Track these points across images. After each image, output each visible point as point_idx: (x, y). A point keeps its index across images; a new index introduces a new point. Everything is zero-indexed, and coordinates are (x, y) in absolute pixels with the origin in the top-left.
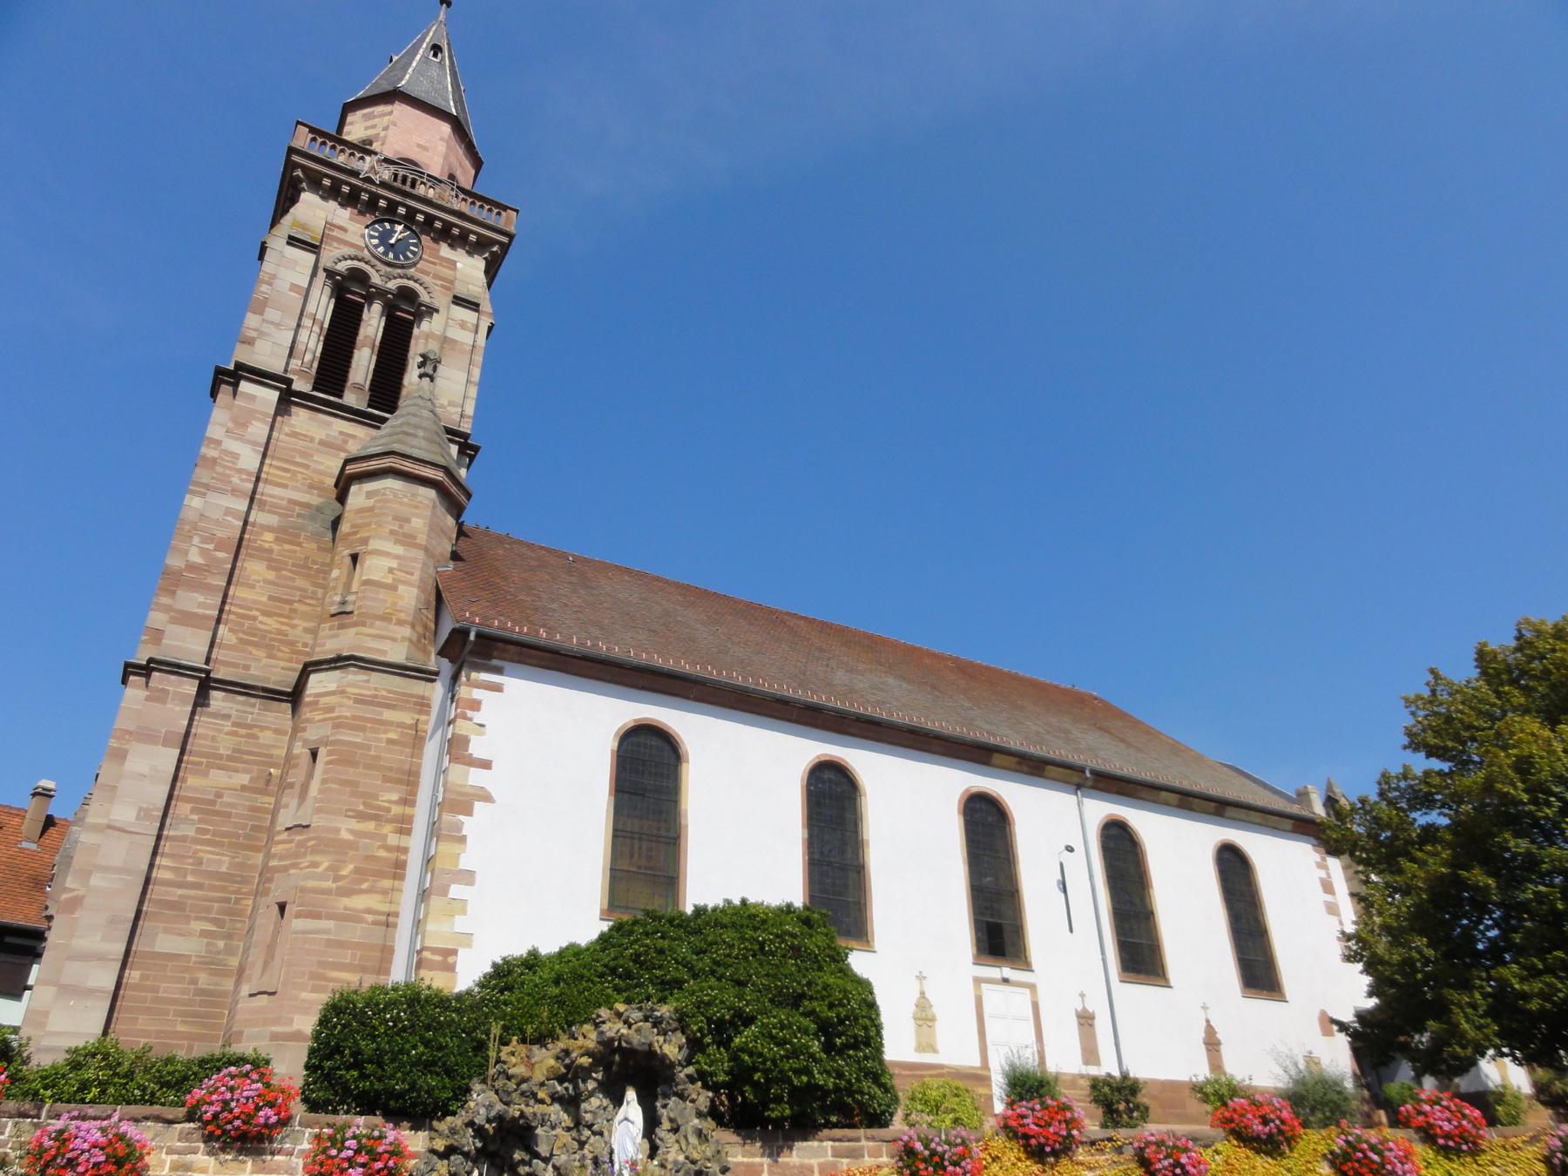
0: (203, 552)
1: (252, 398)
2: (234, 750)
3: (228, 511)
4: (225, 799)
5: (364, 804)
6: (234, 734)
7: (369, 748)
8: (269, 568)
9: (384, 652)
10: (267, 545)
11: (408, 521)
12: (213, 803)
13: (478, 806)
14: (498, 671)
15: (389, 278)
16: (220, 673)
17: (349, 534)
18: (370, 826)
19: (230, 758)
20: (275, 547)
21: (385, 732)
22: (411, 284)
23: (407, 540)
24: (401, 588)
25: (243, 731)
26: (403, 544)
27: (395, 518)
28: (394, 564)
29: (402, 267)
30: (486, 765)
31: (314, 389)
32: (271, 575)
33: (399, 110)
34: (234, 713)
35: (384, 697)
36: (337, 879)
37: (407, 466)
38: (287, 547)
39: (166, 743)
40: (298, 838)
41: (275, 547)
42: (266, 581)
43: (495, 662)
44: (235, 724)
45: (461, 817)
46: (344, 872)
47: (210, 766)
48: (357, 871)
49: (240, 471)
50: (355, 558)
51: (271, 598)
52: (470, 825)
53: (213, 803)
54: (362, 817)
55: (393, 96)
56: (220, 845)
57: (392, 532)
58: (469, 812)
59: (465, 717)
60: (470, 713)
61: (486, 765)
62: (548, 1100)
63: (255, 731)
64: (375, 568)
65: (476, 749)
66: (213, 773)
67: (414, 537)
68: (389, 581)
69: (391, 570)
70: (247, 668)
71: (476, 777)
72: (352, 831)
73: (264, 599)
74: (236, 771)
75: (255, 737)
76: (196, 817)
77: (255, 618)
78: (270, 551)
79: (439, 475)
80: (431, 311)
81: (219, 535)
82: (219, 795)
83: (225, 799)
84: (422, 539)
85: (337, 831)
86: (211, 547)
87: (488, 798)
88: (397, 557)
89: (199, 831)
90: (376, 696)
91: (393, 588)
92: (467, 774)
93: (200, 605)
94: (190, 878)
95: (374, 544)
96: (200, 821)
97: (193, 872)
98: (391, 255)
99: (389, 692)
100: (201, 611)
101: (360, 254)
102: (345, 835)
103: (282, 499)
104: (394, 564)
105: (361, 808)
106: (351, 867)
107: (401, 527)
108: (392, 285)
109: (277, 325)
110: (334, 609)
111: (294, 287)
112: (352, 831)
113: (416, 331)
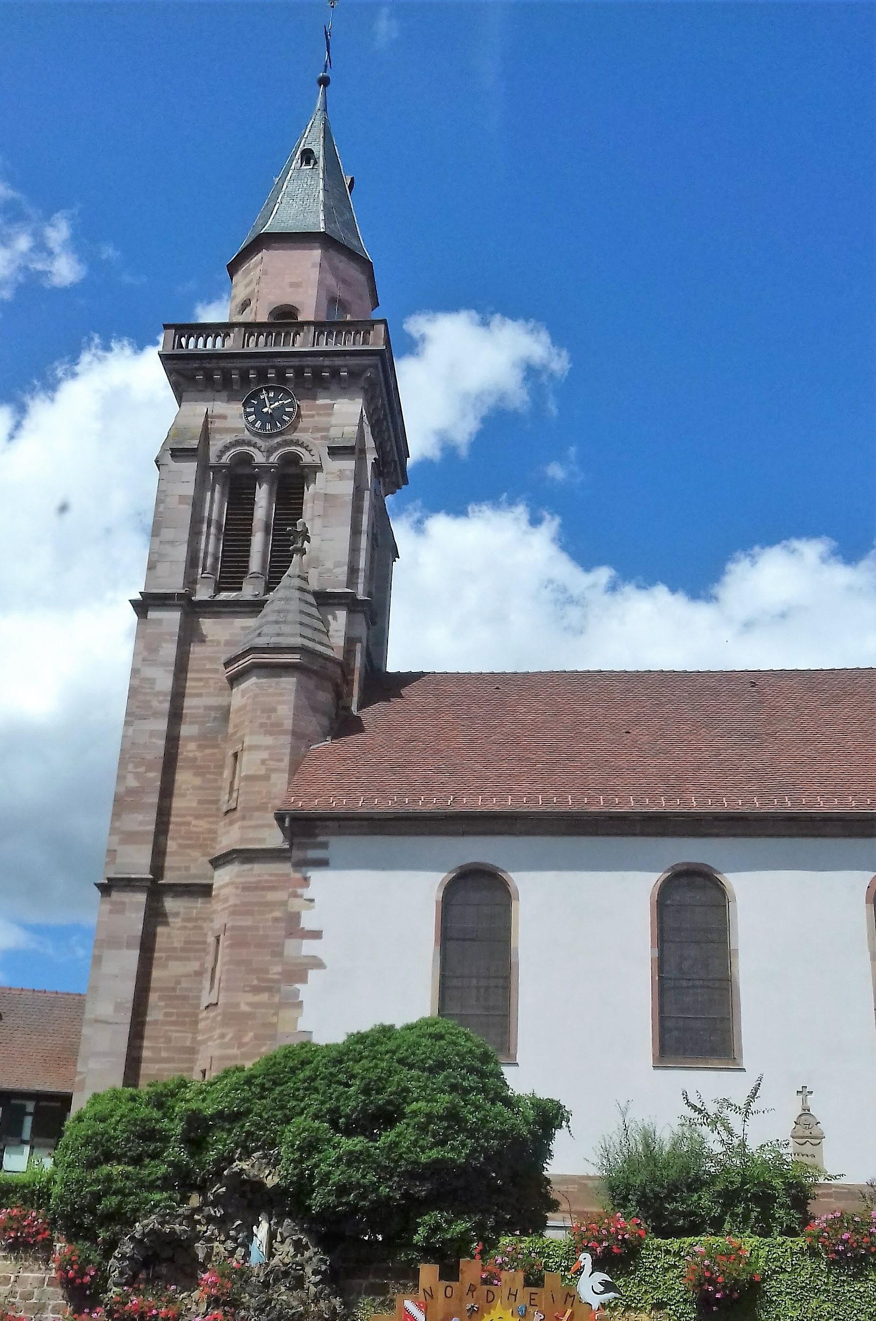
0: (137, 776)
1: (159, 622)
2: (187, 942)
3: (152, 734)
4: (184, 985)
5: (258, 979)
6: (185, 928)
7: (257, 928)
8: (196, 775)
9: (263, 840)
10: (191, 755)
11: (274, 710)
12: (174, 989)
13: (312, 974)
14: (324, 846)
15: (270, 452)
16: (169, 878)
17: (235, 733)
18: (264, 997)
19: (183, 950)
20: (198, 754)
21: (271, 911)
22: (293, 448)
23: (272, 729)
24: (274, 776)
25: (190, 925)
26: (271, 734)
27: (263, 711)
28: (265, 755)
29: (281, 433)
30: (316, 935)
31: (218, 589)
32: (198, 781)
33: (265, 257)
34: (182, 910)
35: (267, 881)
36: (241, 1045)
37: (267, 658)
38: (208, 751)
39: (129, 946)
40: (212, 1015)
41: (198, 754)
42: (195, 788)
43: (321, 839)
44: (184, 920)
45: (297, 986)
46: (246, 1039)
47: (168, 958)
48: (256, 1037)
49: (158, 694)
50: (236, 755)
51: (200, 802)
52: (305, 991)
53: (174, 989)
54: (256, 990)
55: (264, 241)
56: (184, 1024)
57: (262, 725)
58: (303, 979)
59: (295, 895)
60: (300, 891)
61: (316, 935)
62: (204, 1221)
63: (200, 923)
64: (249, 764)
65: (308, 922)
66: (171, 964)
67: (281, 725)
68: (262, 771)
69: (263, 762)
70: (187, 868)
71: (309, 947)
72: (249, 1004)
73: (194, 804)
74: (188, 959)
75: (200, 928)
76: (163, 1004)
77: (189, 823)
78: (195, 759)
79: (294, 658)
80: (319, 468)
81: (148, 757)
82: (178, 982)
83: (184, 985)
84: (288, 724)
85: (237, 1005)
86: (142, 770)
87: (318, 964)
88: (267, 748)
89: (167, 1014)
90: (259, 882)
91: (266, 778)
92: (299, 947)
93: (141, 823)
94: (164, 1054)
95: (247, 741)
96: (166, 1006)
97: (167, 1049)
98: (268, 427)
99: (271, 875)
100: (141, 828)
101: (241, 436)
102: (244, 1008)
103: (198, 708)
104: (265, 755)
105: (255, 982)
106: (251, 1034)
107: (269, 718)
108: (274, 458)
109: (172, 543)
110: (225, 808)
111: (182, 499)
112: (249, 1004)
113: (309, 492)
